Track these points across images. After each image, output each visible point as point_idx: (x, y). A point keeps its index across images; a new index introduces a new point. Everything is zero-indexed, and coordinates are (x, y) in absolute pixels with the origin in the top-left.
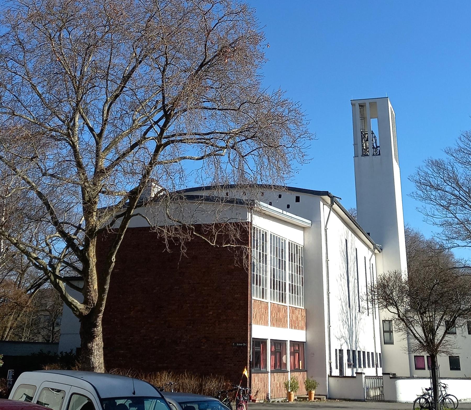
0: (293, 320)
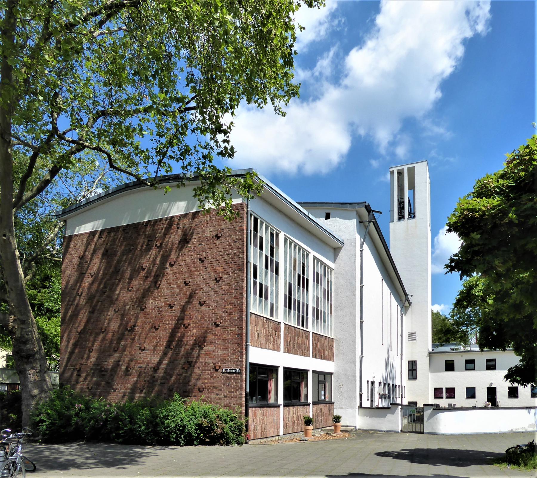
0: (317, 349)
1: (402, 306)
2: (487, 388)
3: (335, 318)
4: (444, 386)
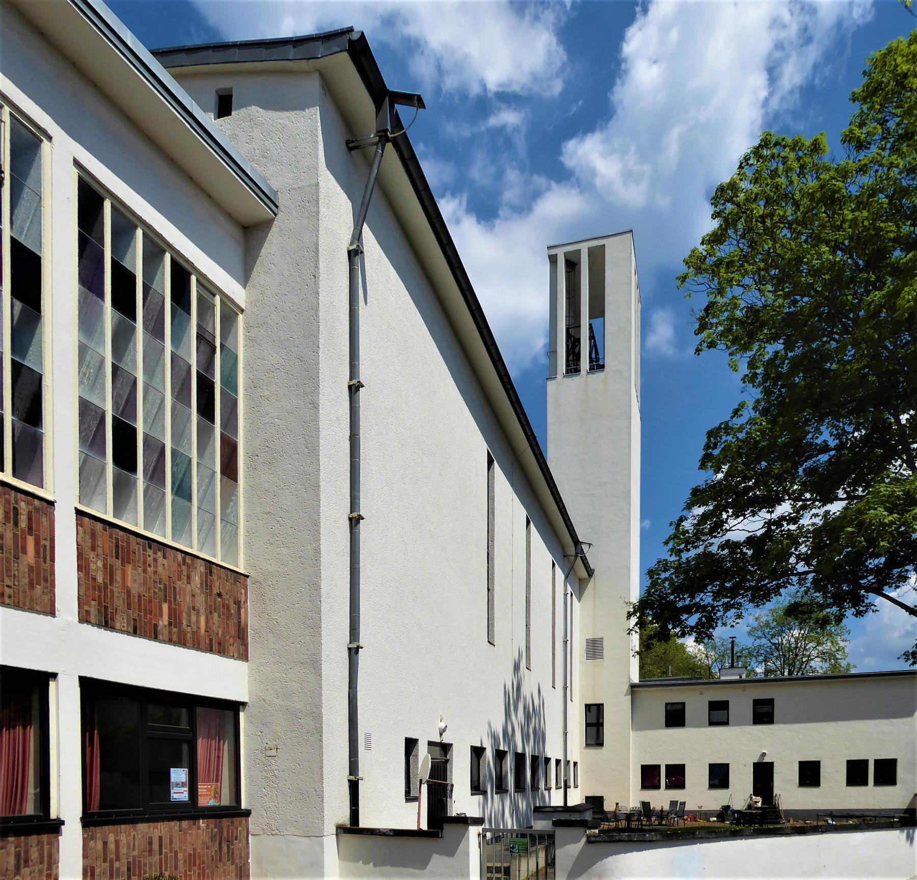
1: (567, 571)
2: (754, 764)
3: (248, 500)
4: (663, 760)
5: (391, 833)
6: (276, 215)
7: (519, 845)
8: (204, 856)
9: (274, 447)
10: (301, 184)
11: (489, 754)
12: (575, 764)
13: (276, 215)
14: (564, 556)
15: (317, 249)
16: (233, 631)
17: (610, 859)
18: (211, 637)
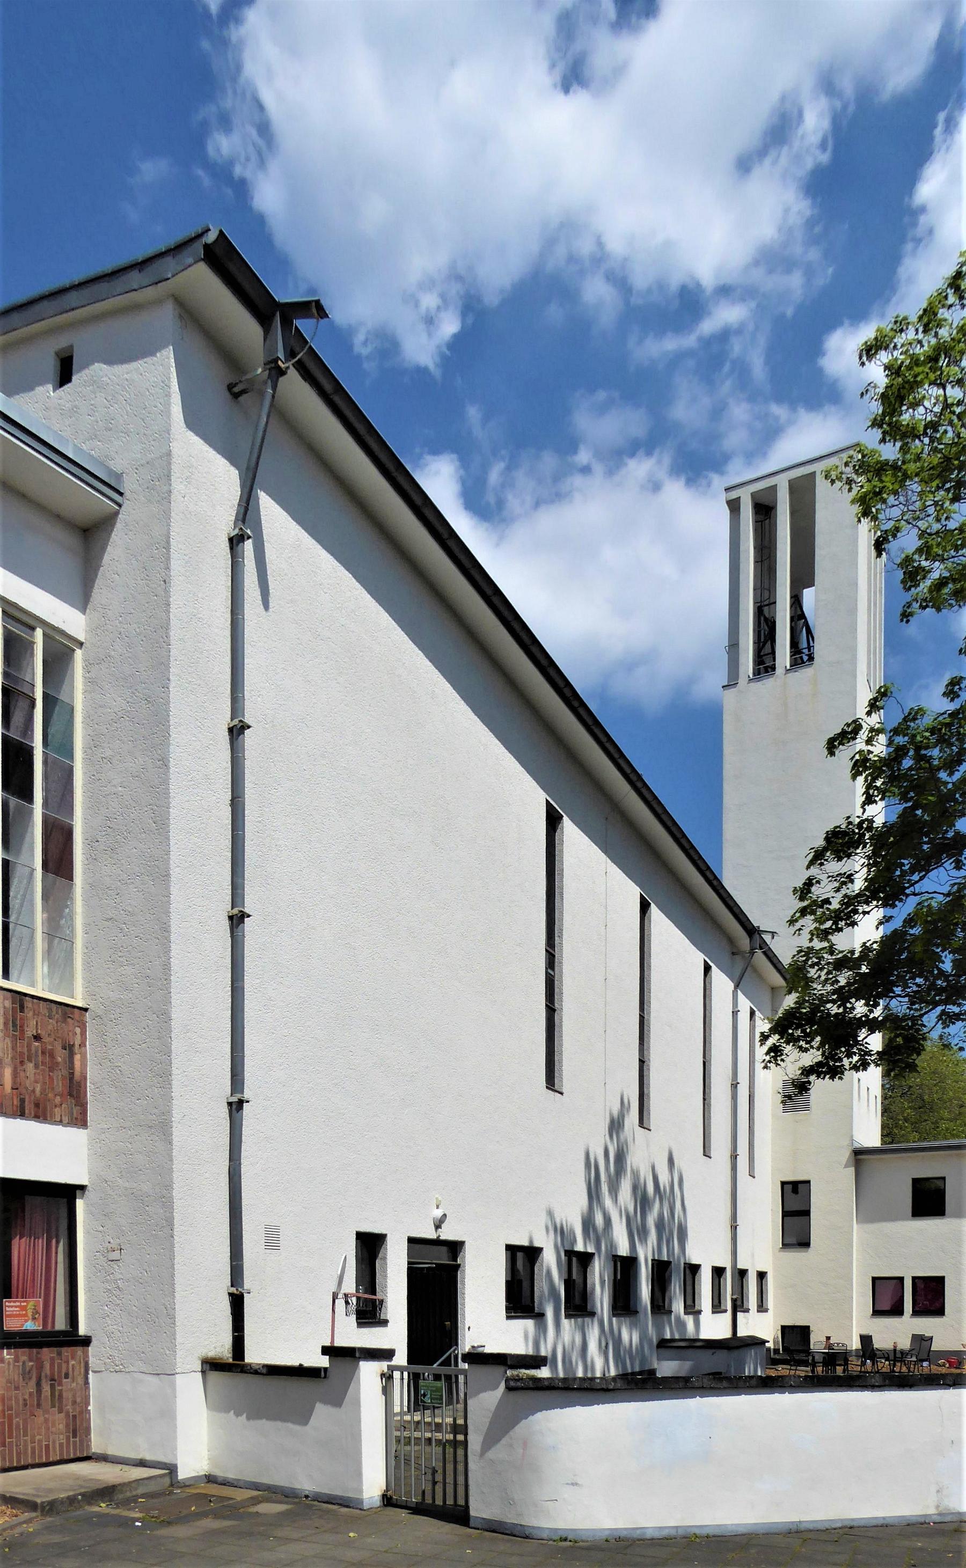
3: (86, 901)
5: (264, 1371)
6: (120, 506)
7: (431, 1391)
8: (10, 1399)
9: (117, 827)
10: (150, 456)
11: (550, 1259)
12: (762, 1276)
13: (120, 506)
14: (733, 954)
15: (168, 542)
16: (59, 1086)
17: (539, 1416)
18: (22, 1097)
